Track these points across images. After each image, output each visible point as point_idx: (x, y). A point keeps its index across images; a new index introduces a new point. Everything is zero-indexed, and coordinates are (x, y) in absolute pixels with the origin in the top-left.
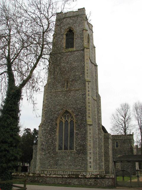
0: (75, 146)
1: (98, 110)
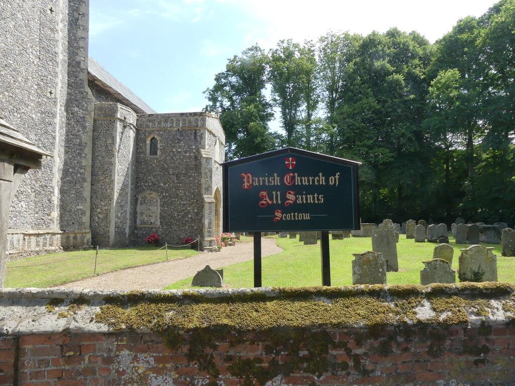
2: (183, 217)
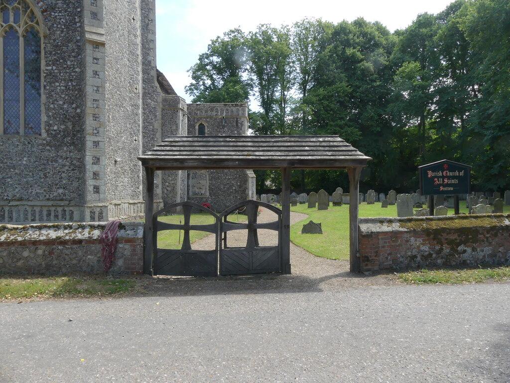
0: (44, 118)
1: (147, 21)
2: (228, 189)
